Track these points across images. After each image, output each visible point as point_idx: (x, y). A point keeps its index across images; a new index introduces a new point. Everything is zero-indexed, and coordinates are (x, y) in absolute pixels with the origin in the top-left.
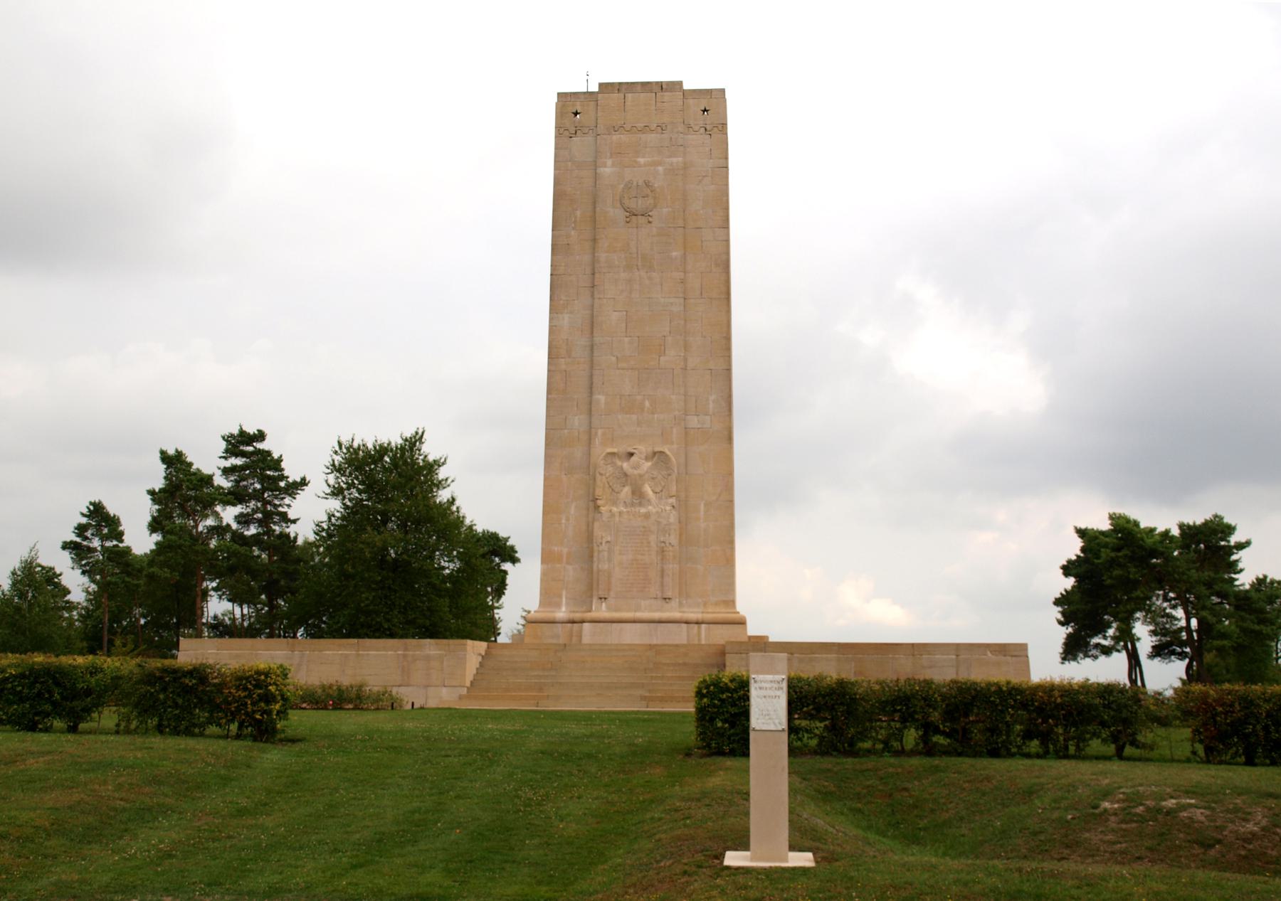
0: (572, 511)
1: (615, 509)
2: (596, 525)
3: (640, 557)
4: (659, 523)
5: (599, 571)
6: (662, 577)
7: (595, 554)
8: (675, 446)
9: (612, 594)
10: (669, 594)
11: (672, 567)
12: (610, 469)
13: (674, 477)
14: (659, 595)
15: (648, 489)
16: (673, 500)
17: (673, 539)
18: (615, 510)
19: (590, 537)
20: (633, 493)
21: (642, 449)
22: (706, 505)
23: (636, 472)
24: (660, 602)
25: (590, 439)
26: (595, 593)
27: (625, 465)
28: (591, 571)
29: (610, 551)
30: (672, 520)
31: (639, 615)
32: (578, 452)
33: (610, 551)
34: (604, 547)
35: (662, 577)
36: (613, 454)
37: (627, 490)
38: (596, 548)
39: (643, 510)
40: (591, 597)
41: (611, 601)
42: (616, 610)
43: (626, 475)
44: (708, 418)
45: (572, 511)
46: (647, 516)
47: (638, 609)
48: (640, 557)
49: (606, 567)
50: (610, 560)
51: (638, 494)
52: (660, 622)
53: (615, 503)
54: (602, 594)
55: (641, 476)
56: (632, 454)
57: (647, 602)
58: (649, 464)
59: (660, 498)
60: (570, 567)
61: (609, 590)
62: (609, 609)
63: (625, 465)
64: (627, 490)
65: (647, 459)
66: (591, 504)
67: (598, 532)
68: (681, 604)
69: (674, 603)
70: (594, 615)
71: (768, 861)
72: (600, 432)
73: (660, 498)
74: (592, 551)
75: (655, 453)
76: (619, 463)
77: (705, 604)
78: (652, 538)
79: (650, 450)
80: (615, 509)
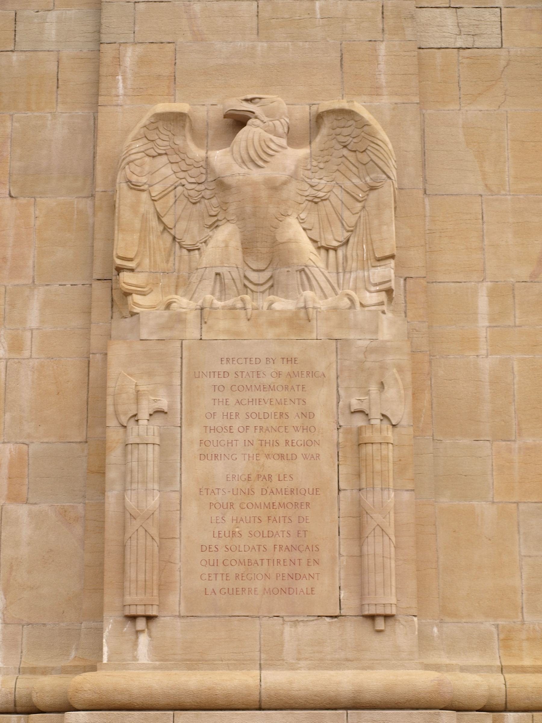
0: (33, 318)
1: (183, 303)
2: (118, 352)
3: (275, 466)
4: (341, 345)
5: (124, 511)
6: (360, 535)
7: (114, 456)
8: (385, 101)
9: (174, 601)
10: (387, 599)
11: (391, 502)
12: (165, 171)
13: (387, 192)
14: (350, 606)
15: (295, 232)
16: (386, 272)
17: (395, 401)
18: (184, 303)
19: (94, 403)
20: (248, 247)
21: (281, 106)
22: (494, 295)
23: (256, 175)
24: (353, 631)
25: (97, 83)
26: (110, 598)
27: (219, 157)
28: (96, 523)
29: (166, 445)
30: (386, 333)
31: (276, 680)
32: (57, 125)
33: (166, 445)
34: (147, 429)
35: (360, 535)
36: (178, 118)
37: (227, 235)
38: (114, 435)
39: (283, 305)
40: (98, 614)
41: (170, 627)
42: (191, 664)
43: (221, 185)
44: (492, 16)
45: (33, 318)
46: (300, 320)
47: (271, 658)
48: (275, 466)
49: (153, 501)
50: (164, 480)
51: (267, 255)
52: (357, 705)
53: (182, 284)
54: (137, 600)
55: (274, 187)
56: (238, 121)
57: (308, 630)
58: (303, 152)
59: (342, 268)
60: (22, 511)
61: (164, 587)
62: (163, 658)
63: (219, 157)
64: (227, 235)
65: (293, 138)
66: (100, 290)
67: (124, 374)
68: (424, 641)
69: (402, 635)
70: (105, 680)
71: (320, 713)
72: (130, 56)
73: (342, 268)
74: (101, 450)
75: (319, 119)
76: (197, 152)
77: (507, 641)
78: (321, 398)
79: (302, 112)
80: (183, 303)
